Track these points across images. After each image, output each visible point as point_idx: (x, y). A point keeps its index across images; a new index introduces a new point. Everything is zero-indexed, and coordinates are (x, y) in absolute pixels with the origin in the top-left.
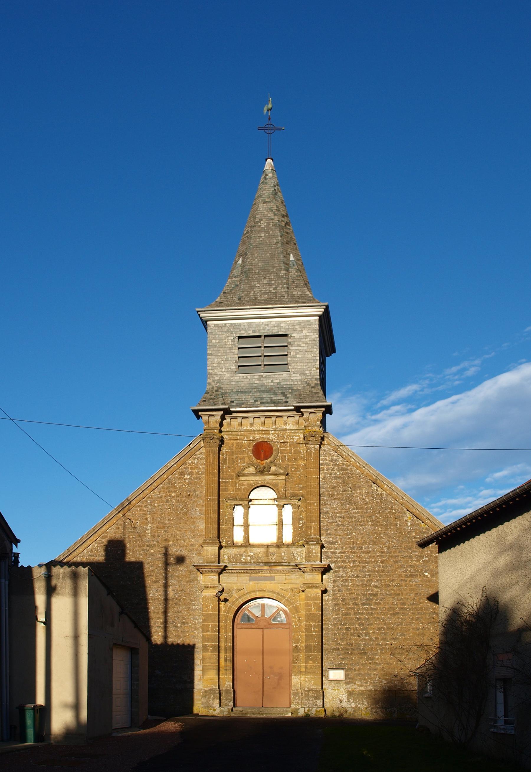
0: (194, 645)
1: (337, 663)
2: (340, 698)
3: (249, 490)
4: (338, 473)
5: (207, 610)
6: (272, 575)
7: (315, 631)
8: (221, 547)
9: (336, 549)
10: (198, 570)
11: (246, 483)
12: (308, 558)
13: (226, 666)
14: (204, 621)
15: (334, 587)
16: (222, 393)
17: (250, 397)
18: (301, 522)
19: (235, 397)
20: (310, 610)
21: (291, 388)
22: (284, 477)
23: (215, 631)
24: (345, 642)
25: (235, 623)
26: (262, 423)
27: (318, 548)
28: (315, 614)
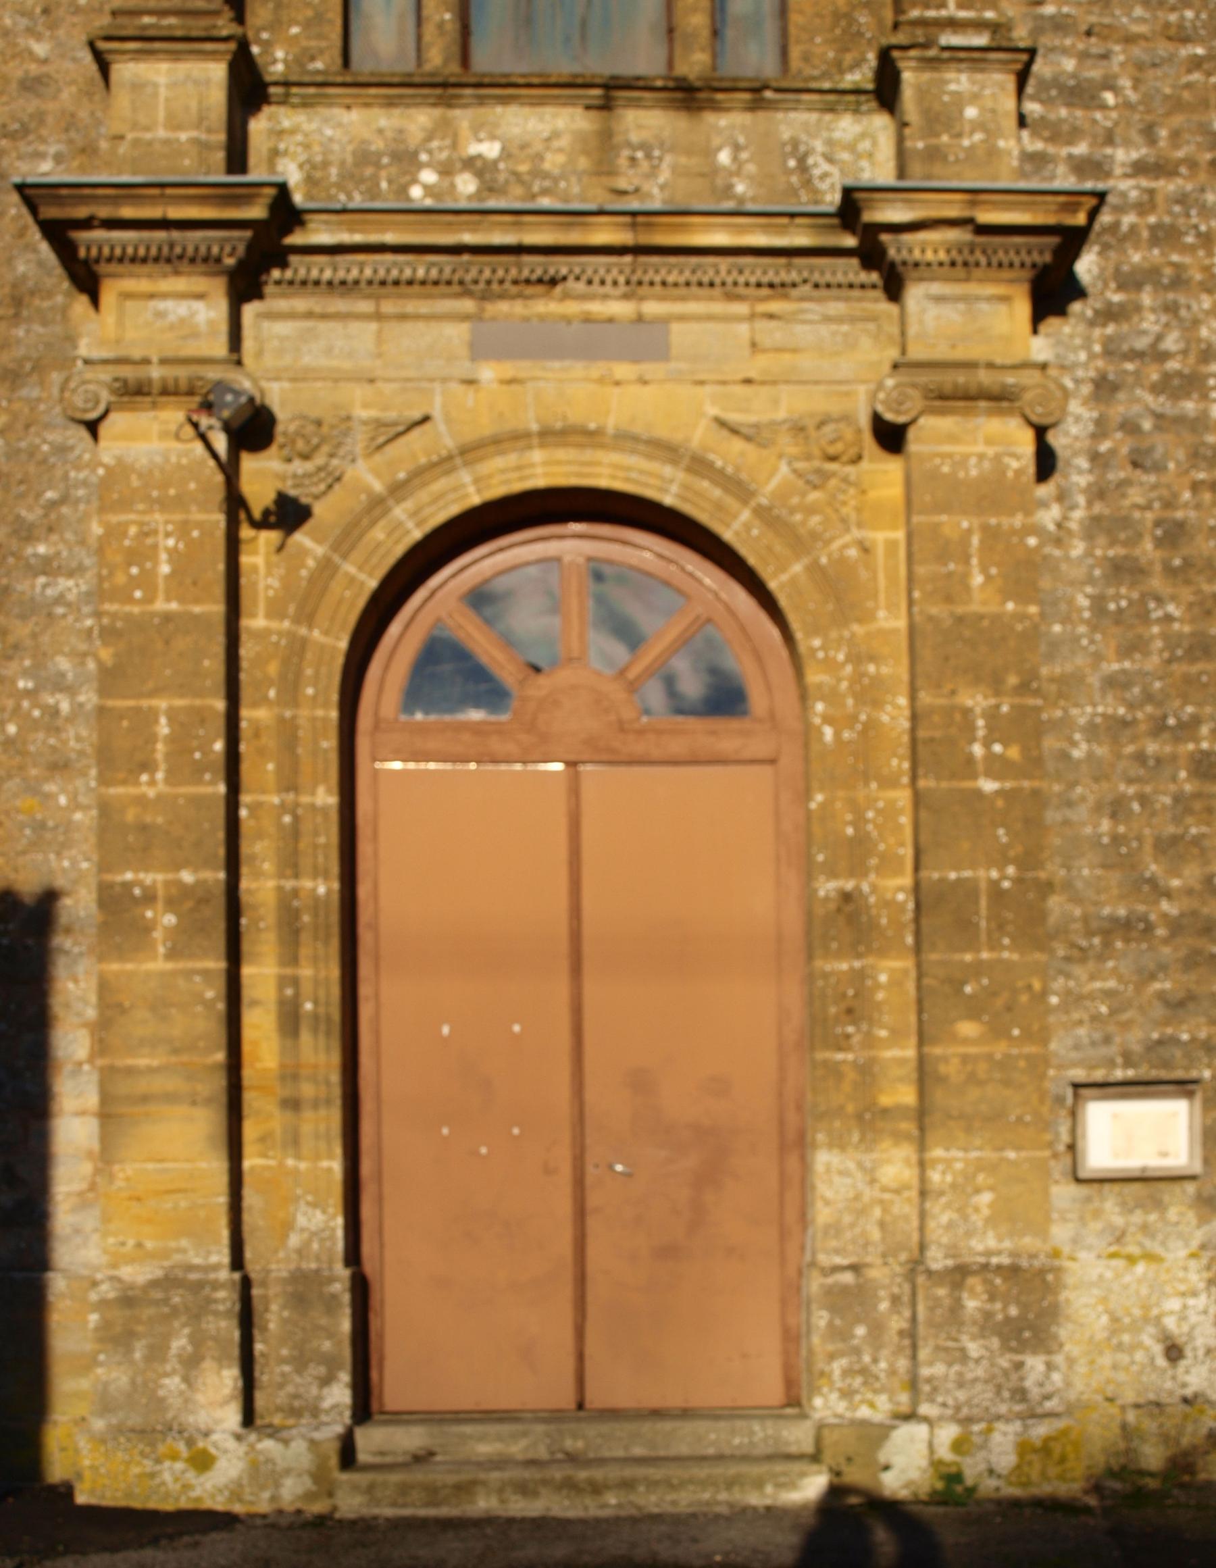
0: (50, 897)
1: (1134, 1039)
2: (1170, 1323)
5: (134, 582)
6: (652, 308)
7: (997, 766)
9: (1109, 139)
10: (58, 234)
13: (290, 1074)
14: (109, 680)
15: (1101, 429)
20: (952, 589)
23: (197, 771)
24: (1192, 873)
25: (364, 721)
28: (996, 618)
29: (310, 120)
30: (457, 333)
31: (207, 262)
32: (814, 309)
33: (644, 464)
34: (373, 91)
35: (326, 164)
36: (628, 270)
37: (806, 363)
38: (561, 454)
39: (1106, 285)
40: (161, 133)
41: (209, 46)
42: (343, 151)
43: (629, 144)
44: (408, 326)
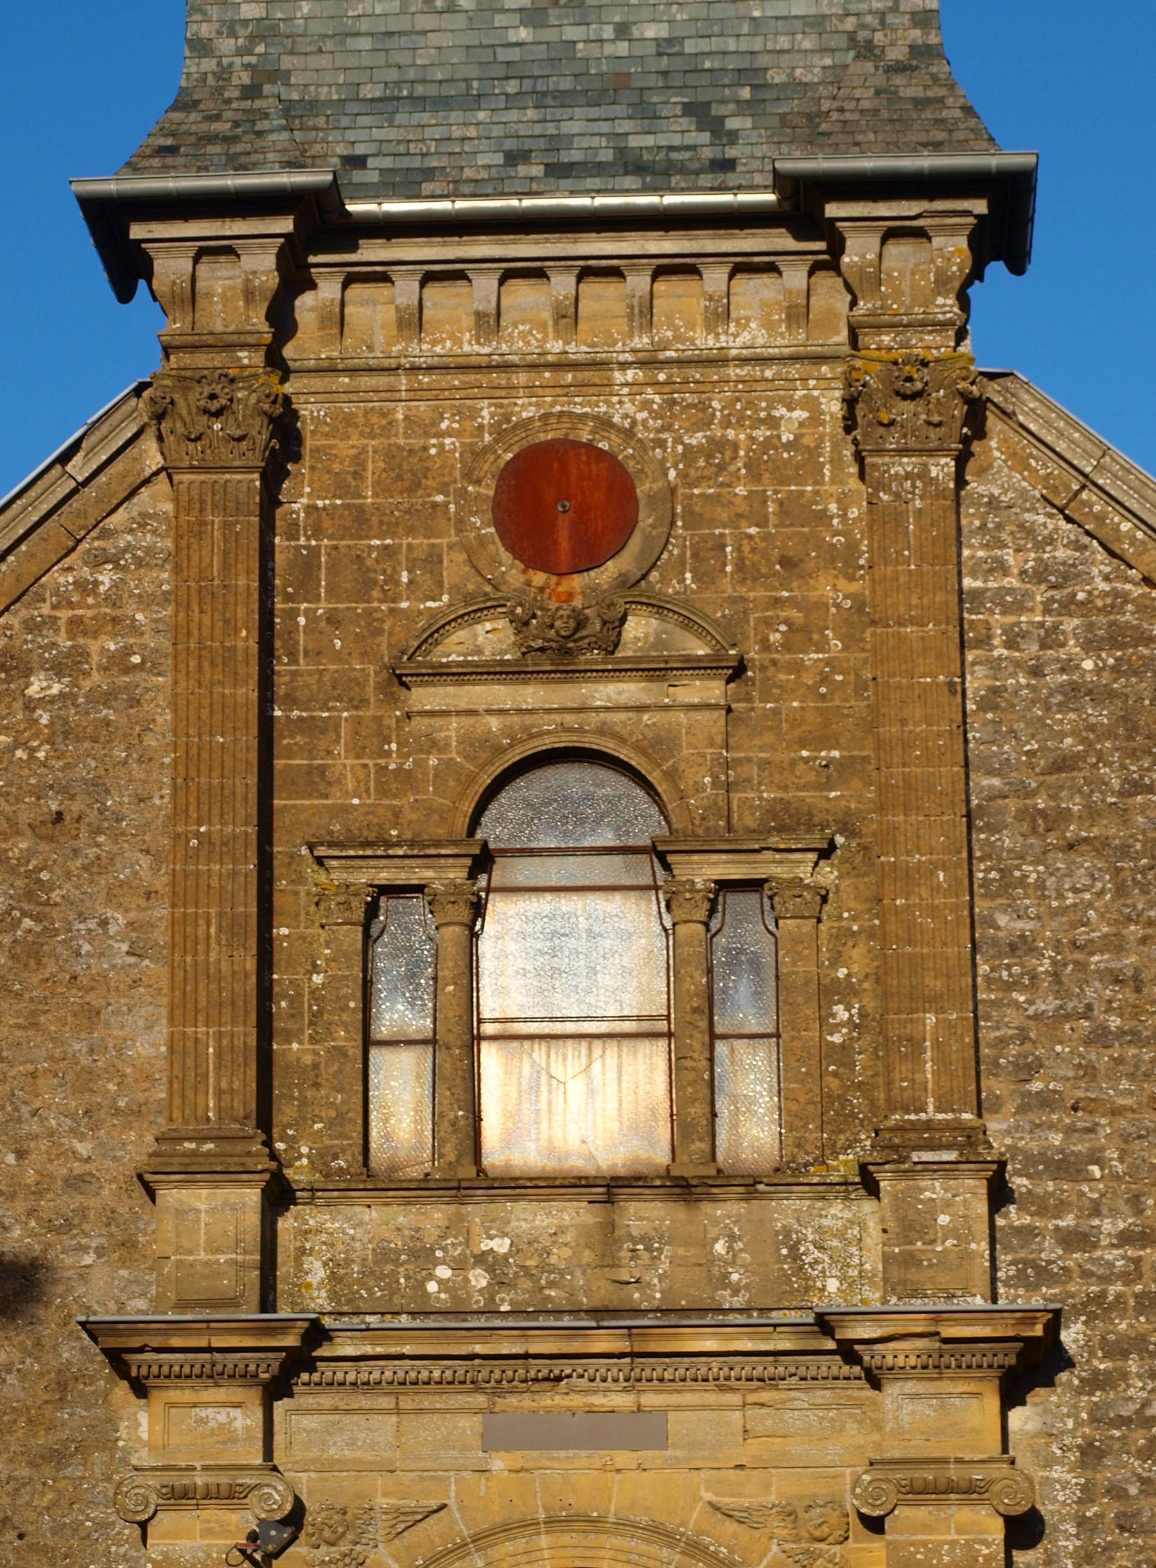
3: (472, 779)
4: (1088, 665)
6: (650, 1400)
8: (279, 1196)
10: (117, 1360)
11: (452, 728)
12: (901, 1272)
15: (1088, 1494)
16: (288, 108)
17: (478, 135)
18: (841, 1013)
19: (377, 134)
21: (750, 75)
22: (714, 690)
26: (560, 316)
27: (972, 1193)
29: (333, 1220)
30: (470, 1425)
31: (246, 1378)
32: (802, 1399)
33: (643, 1547)
34: (392, 1193)
35: (348, 1262)
36: (627, 1369)
37: (795, 1447)
38: (566, 1539)
39: (1092, 1354)
40: (203, 1256)
41: (245, 1177)
42: (363, 1249)
43: (631, 1238)
44: (425, 1419)
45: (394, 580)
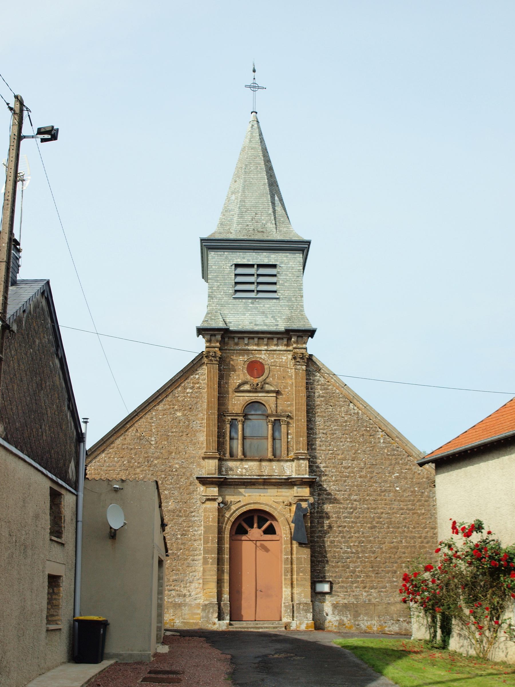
5: (208, 521)
22: (274, 395)
45: (234, 378)
